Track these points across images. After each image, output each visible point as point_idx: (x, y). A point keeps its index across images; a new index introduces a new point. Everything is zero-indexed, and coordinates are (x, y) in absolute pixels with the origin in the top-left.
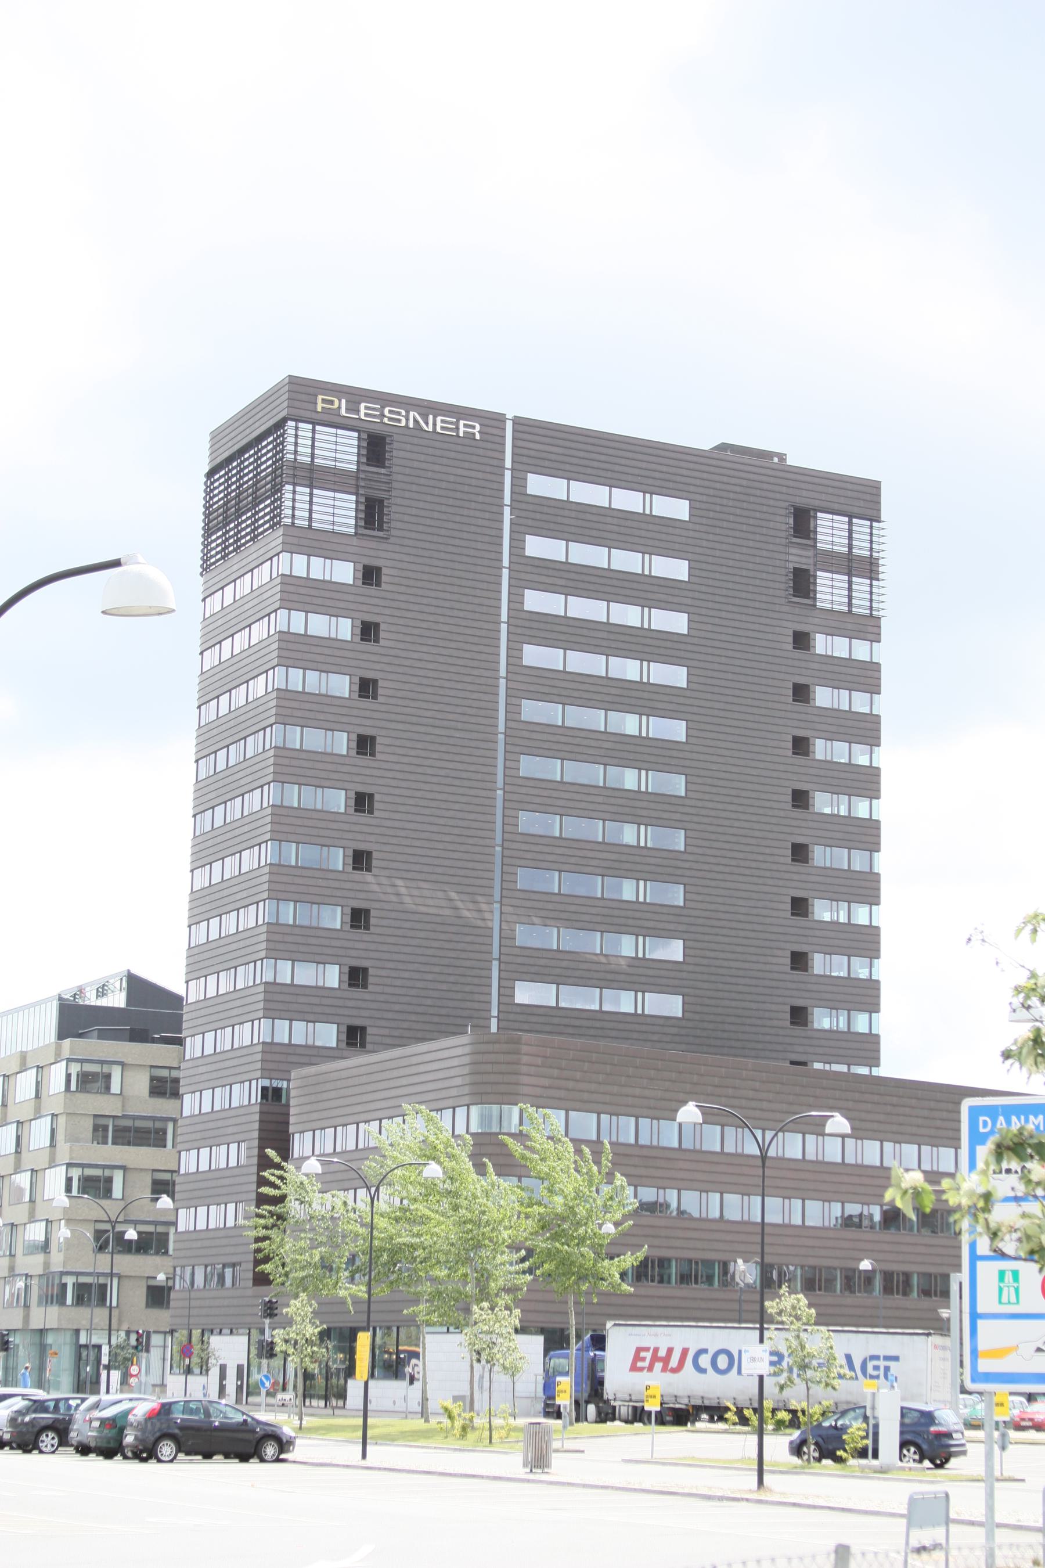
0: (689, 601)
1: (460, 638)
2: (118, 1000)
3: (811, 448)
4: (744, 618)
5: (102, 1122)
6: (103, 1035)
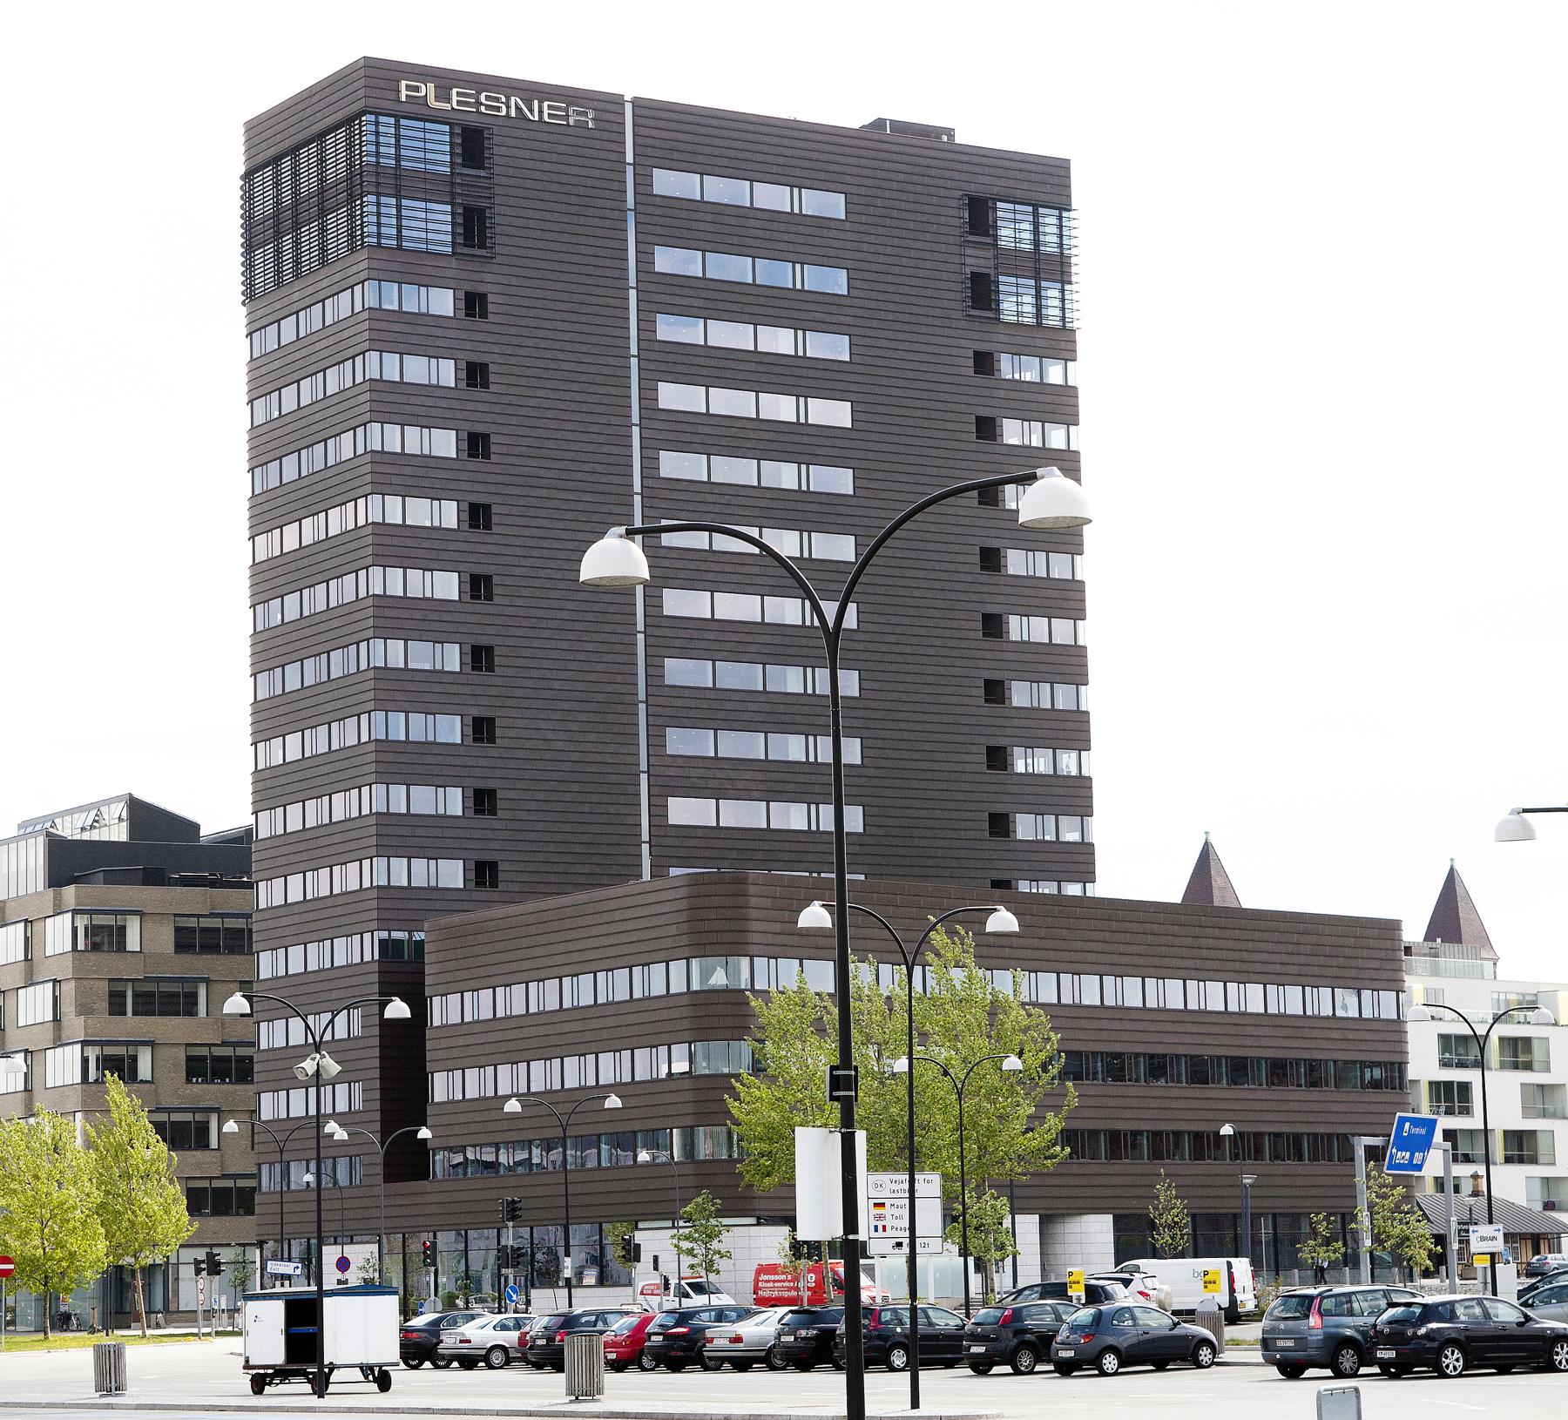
0: (850, 320)
1: (584, 378)
2: (118, 833)
3: (981, 126)
4: (915, 338)
5: (118, 987)
6: (111, 879)
